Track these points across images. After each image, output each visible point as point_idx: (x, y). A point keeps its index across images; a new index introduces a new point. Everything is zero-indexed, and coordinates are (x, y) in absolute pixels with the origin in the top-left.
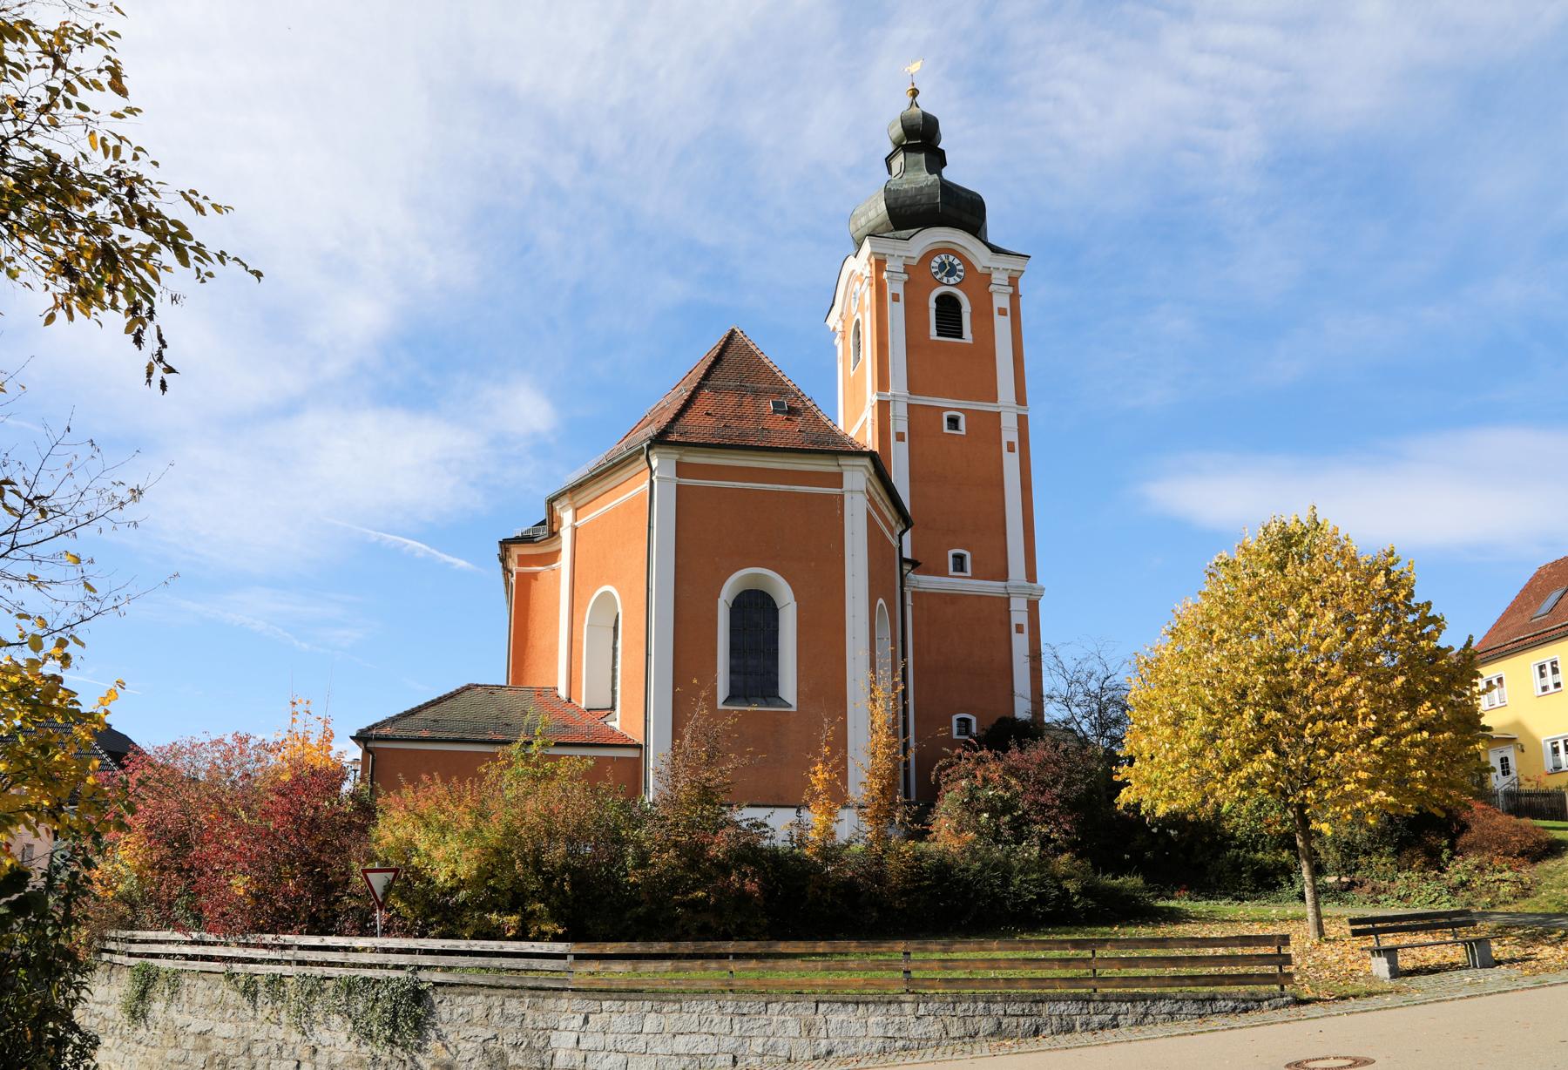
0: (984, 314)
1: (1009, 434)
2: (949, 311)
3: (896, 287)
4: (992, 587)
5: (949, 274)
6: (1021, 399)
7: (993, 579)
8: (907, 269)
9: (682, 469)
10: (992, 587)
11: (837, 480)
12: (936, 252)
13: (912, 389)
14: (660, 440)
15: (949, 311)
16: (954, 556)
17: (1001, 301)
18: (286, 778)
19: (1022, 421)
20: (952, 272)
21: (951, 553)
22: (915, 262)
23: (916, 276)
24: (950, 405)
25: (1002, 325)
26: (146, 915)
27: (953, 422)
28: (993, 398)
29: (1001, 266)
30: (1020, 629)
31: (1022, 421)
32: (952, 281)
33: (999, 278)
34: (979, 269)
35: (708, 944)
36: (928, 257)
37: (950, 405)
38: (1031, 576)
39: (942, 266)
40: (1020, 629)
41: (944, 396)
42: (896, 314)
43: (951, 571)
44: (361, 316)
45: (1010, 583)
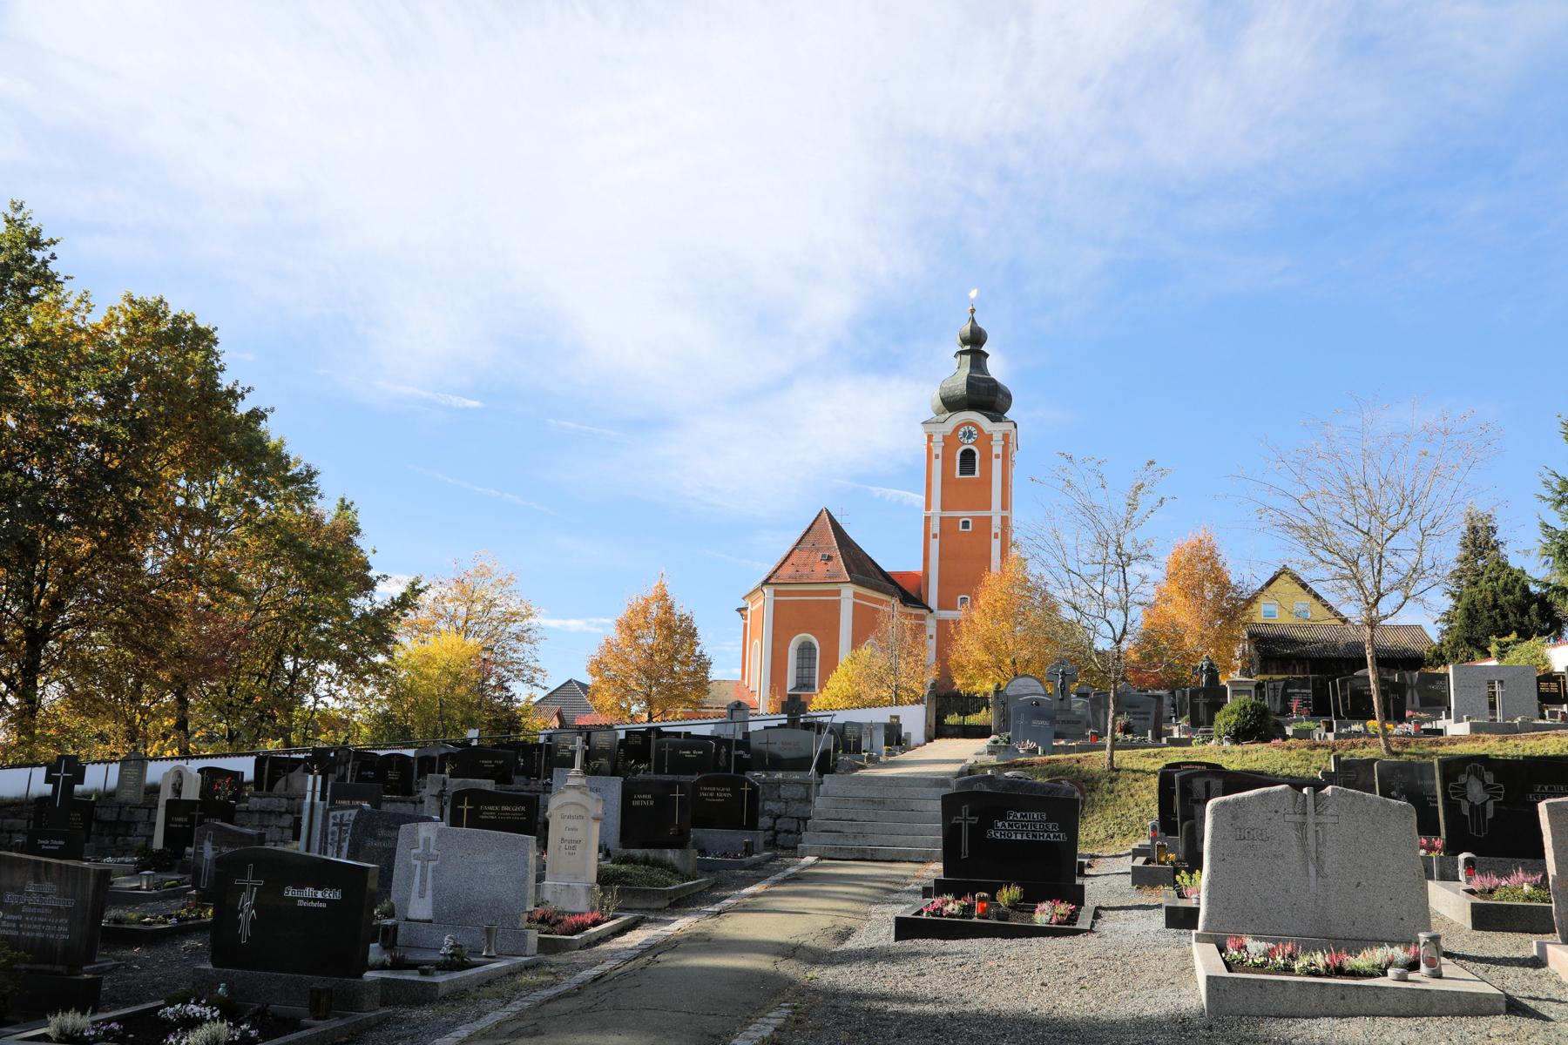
0: (987, 459)
1: (996, 527)
2: (968, 456)
3: (938, 450)
6: (1005, 505)
9: (776, 593)
11: (838, 593)
12: (962, 425)
13: (943, 508)
14: (766, 582)
15: (968, 456)
17: (997, 450)
18: (542, 740)
19: (1005, 520)
20: (971, 435)
23: (949, 441)
24: (963, 514)
25: (997, 464)
26: (1112, 720)
27: (966, 524)
31: (1005, 520)
33: (997, 437)
37: (963, 514)
42: (937, 465)
44: (832, 307)
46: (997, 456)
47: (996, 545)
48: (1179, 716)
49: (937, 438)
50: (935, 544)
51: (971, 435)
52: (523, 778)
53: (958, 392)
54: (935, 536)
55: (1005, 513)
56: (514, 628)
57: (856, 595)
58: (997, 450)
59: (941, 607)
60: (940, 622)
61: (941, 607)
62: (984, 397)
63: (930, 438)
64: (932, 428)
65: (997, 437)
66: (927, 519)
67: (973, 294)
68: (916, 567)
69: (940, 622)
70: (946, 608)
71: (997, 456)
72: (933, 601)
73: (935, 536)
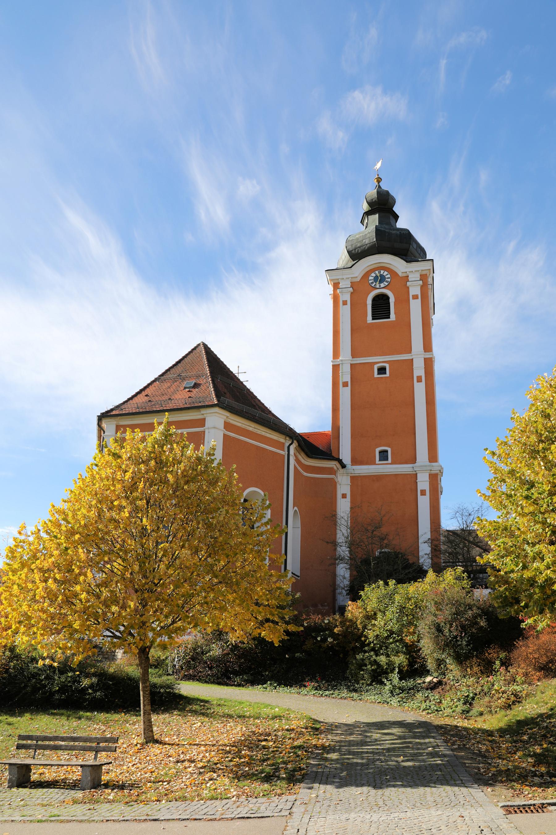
1: (419, 370)
2: (381, 306)
4: (404, 468)
5: (381, 282)
7: (406, 463)
8: (353, 285)
10: (404, 468)
11: (202, 422)
13: (354, 355)
15: (381, 306)
16: (379, 374)
17: (415, 290)
19: (429, 364)
20: (382, 279)
21: (378, 450)
22: (358, 279)
23: (357, 289)
24: (379, 360)
25: (415, 306)
27: (384, 455)
28: (409, 350)
29: (413, 270)
30: (423, 493)
32: (382, 285)
33: (414, 277)
34: (400, 274)
35: (251, 429)
36: (366, 275)
37: (379, 360)
38: (433, 456)
39: (376, 278)
40: (419, 379)
41: (376, 355)
42: (346, 312)
43: (377, 461)
45: (413, 353)
46: (415, 297)
47: (420, 390)
48: (453, 565)
49: (345, 284)
50: (345, 394)
51: (382, 279)
52: (338, 549)
53: (373, 197)
54: (345, 384)
55: (428, 355)
56: (56, 531)
57: (228, 426)
58: (415, 290)
59: (355, 461)
60: (354, 479)
61: (355, 461)
62: (396, 242)
63: (336, 286)
64: (337, 275)
65: (414, 277)
66: (336, 368)
67: (379, 165)
68: (327, 428)
69: (354, 479)
70: (361, 463)
71: (415, 297)
72: (345, 454)
73: (345, 384)
